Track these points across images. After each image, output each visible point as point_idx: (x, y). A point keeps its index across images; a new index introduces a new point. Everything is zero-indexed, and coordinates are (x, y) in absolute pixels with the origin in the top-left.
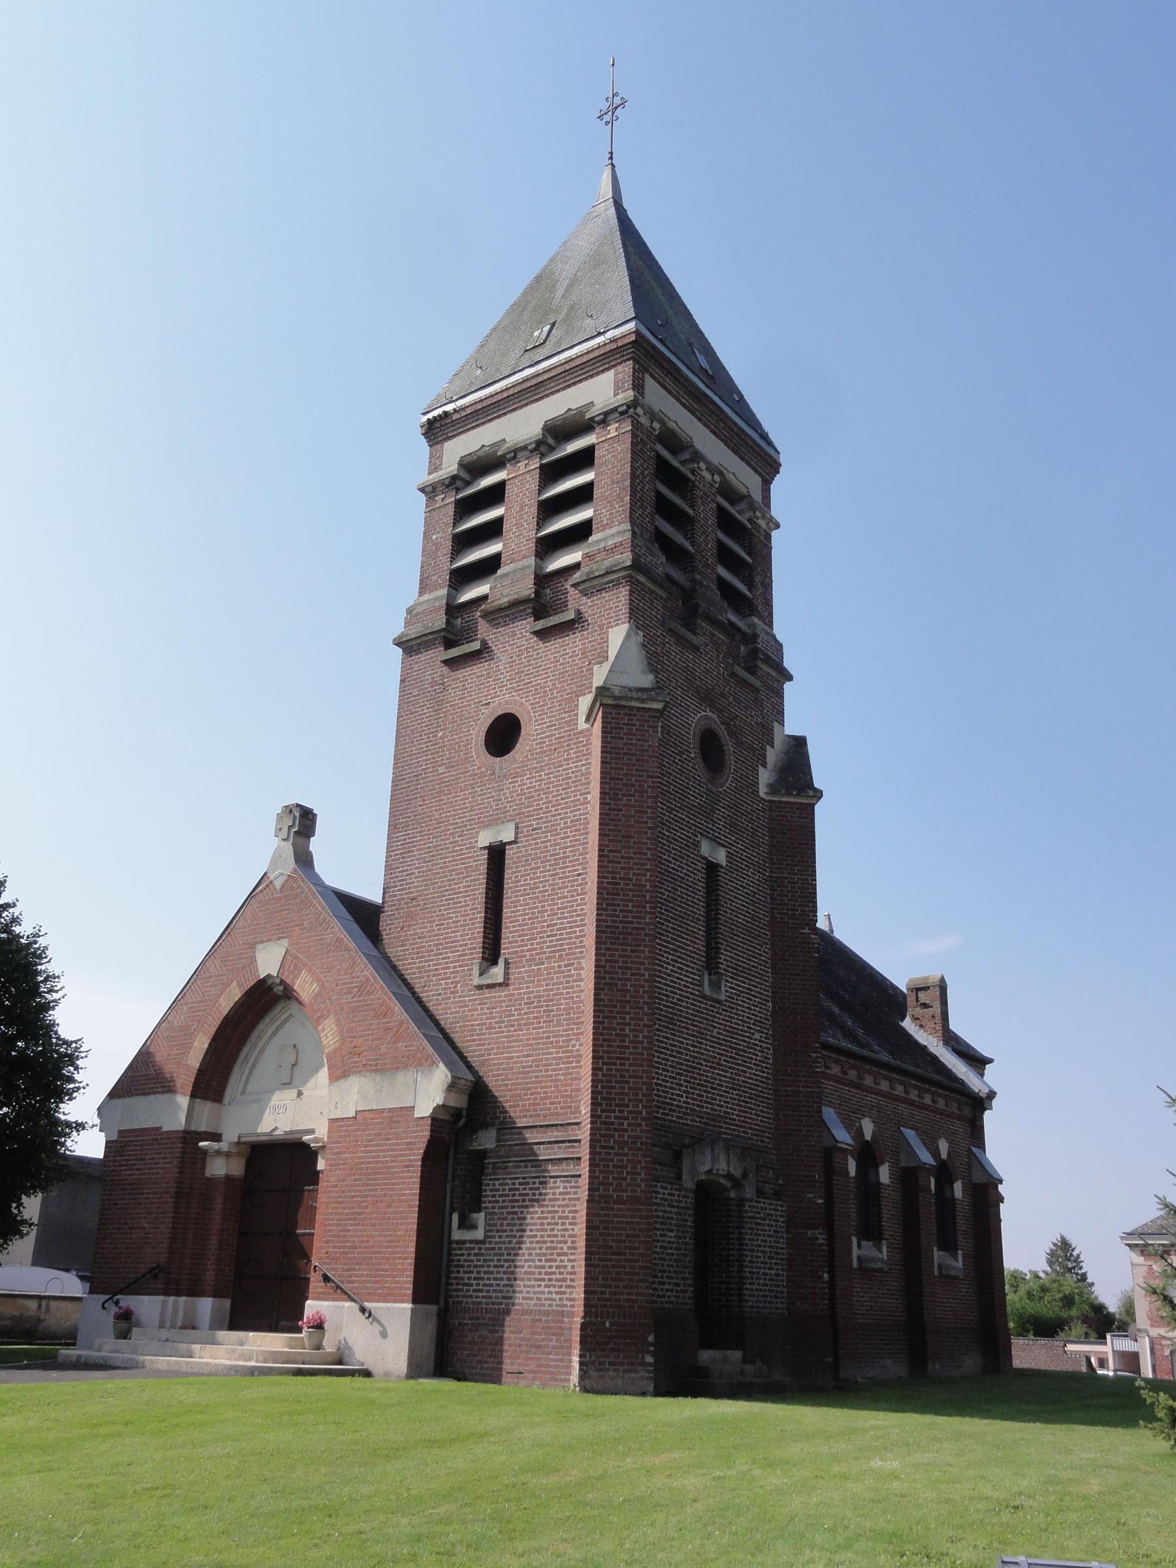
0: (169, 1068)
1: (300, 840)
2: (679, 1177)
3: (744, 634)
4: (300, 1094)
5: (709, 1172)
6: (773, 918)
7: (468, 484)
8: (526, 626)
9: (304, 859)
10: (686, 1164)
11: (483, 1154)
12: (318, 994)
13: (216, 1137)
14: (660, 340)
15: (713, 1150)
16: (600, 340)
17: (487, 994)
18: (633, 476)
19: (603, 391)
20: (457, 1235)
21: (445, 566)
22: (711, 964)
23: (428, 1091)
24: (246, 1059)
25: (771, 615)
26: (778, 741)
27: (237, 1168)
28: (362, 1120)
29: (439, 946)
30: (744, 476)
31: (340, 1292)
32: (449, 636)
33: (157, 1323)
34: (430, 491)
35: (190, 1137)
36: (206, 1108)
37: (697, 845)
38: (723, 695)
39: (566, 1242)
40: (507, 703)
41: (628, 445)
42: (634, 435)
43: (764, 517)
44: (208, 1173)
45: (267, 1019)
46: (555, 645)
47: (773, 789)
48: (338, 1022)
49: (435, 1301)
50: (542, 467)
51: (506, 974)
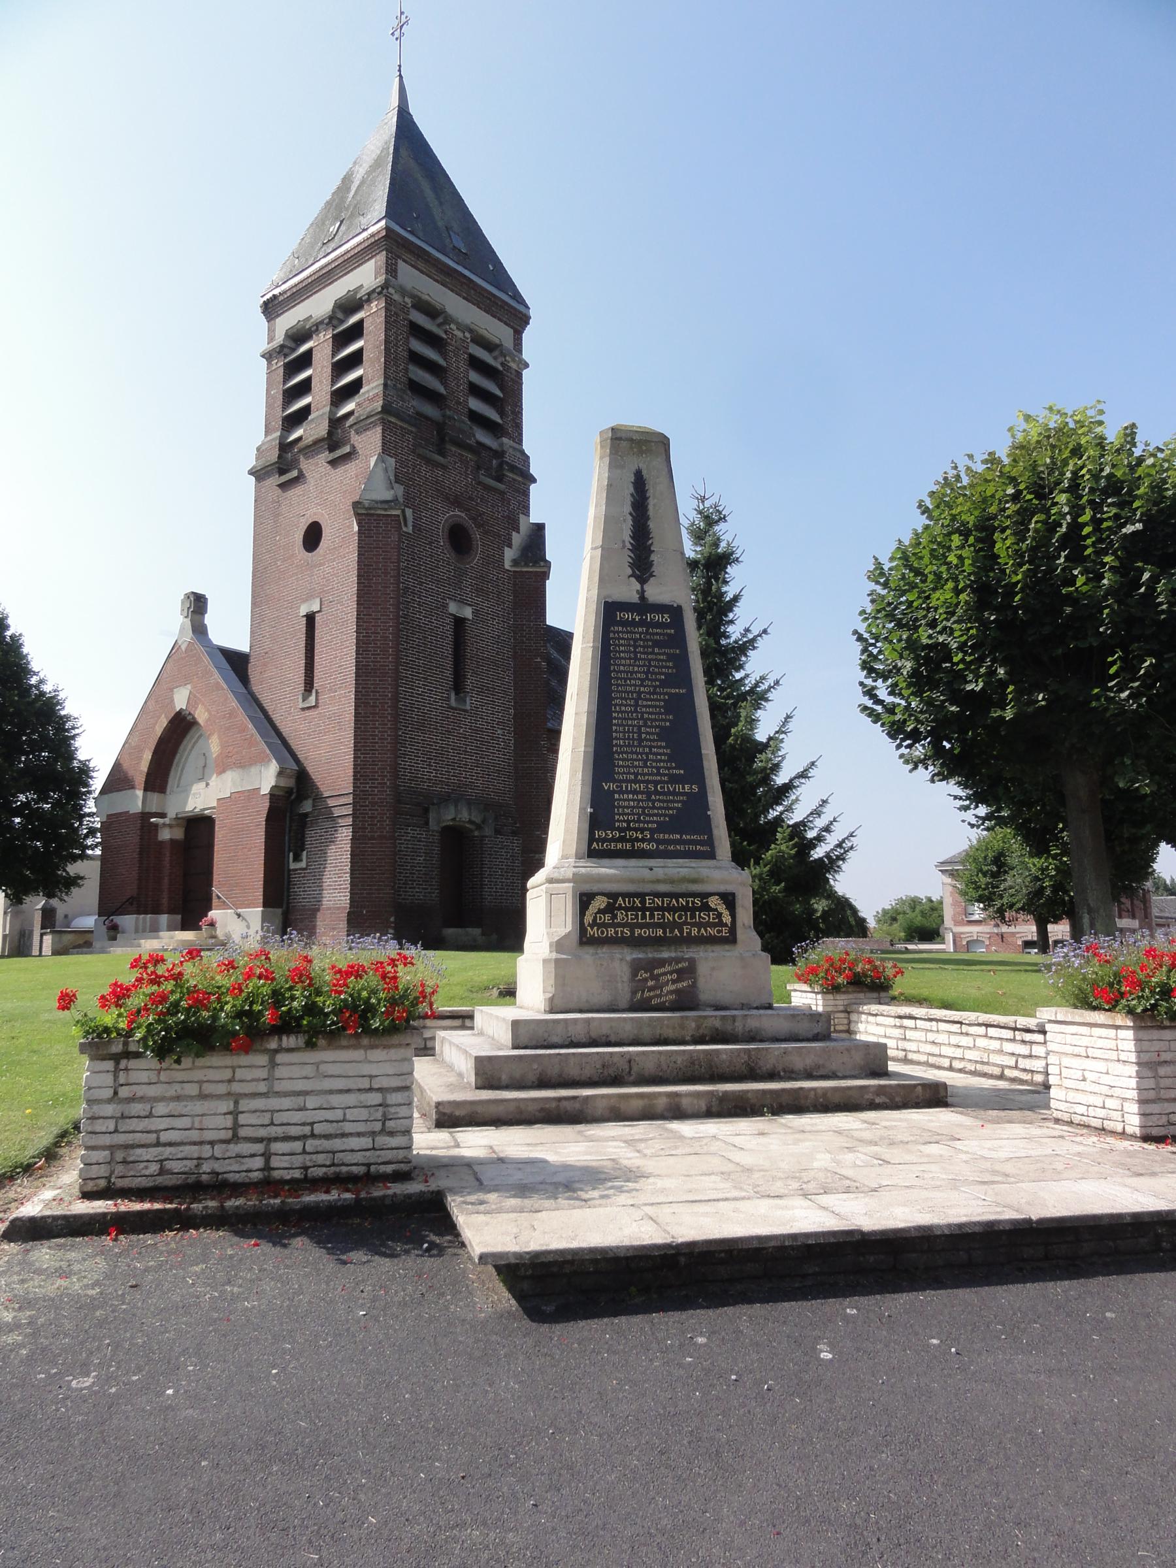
0: (131, 773)
1: (197, 617)
2: (427, 823)
3: (496, 452)
4: (207, 785)
5: (454, 819)
6: (515, 653)
7: (294, 350)
8: (325, 456)
9: (200, 630)
10: (432, 816)
11: (306, 815)
12: (209, 720)
13: (162, 815)
14: (411, 232)
15: (456, 806)
16: (365, 235)
17: (308, 713)
18: (387, 342)
19: (367, 276)
20: (293, 866)
21: (279, 414)
22: (458, 686)
23: (266, 777)
24: (177, 766)
25: (521, 434)
26: (523, 528)
27: (179, 834)
28: (235, 798)
29: (278, 685)
30: (497, 331)
31: (224, 906)
32: (281, 467)
33: (133, 929)
34: (268, 356)
35: (145, 816)
36: (154, 797)
37: (445, 606)
38: (471, 498)
40: (315, 514)
41: (383, 319)
42: (387, 309)
43: (514, 360)
44: (160, 838)
45: (188, 737)
46: (341, 470)
47: (515, 562)
48: (220, 738)
49: (280, 906)
50: (334, 337)
51: (317, 699)
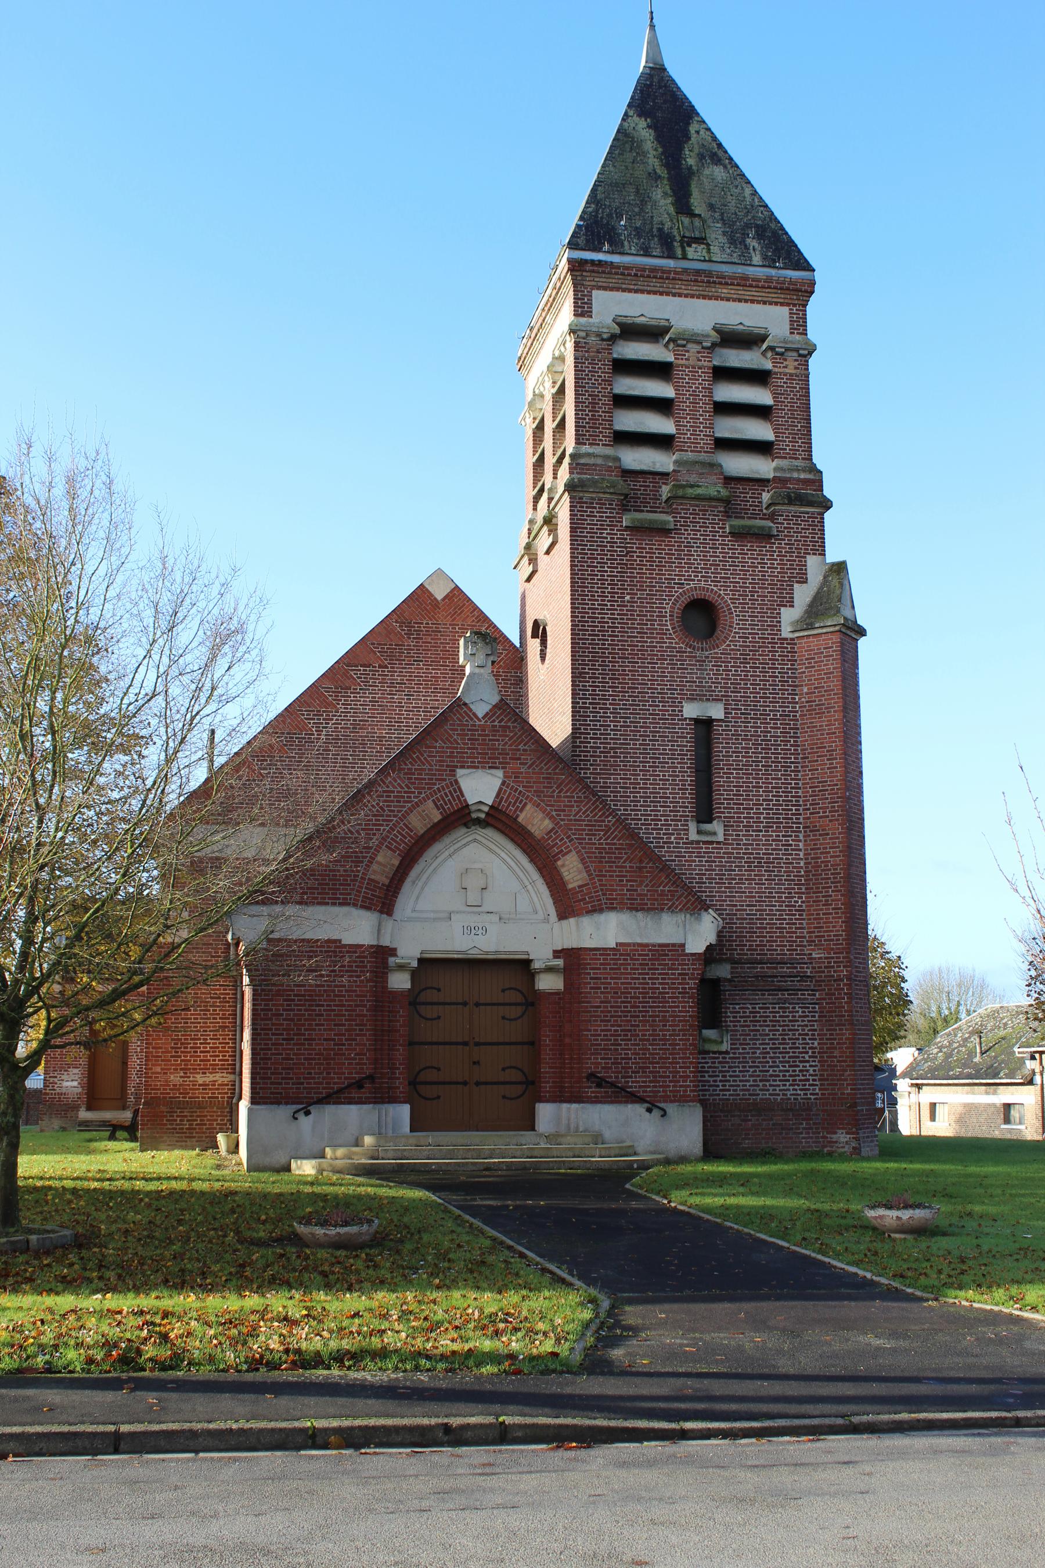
24: (418, 877)
39: (807, 1053)
